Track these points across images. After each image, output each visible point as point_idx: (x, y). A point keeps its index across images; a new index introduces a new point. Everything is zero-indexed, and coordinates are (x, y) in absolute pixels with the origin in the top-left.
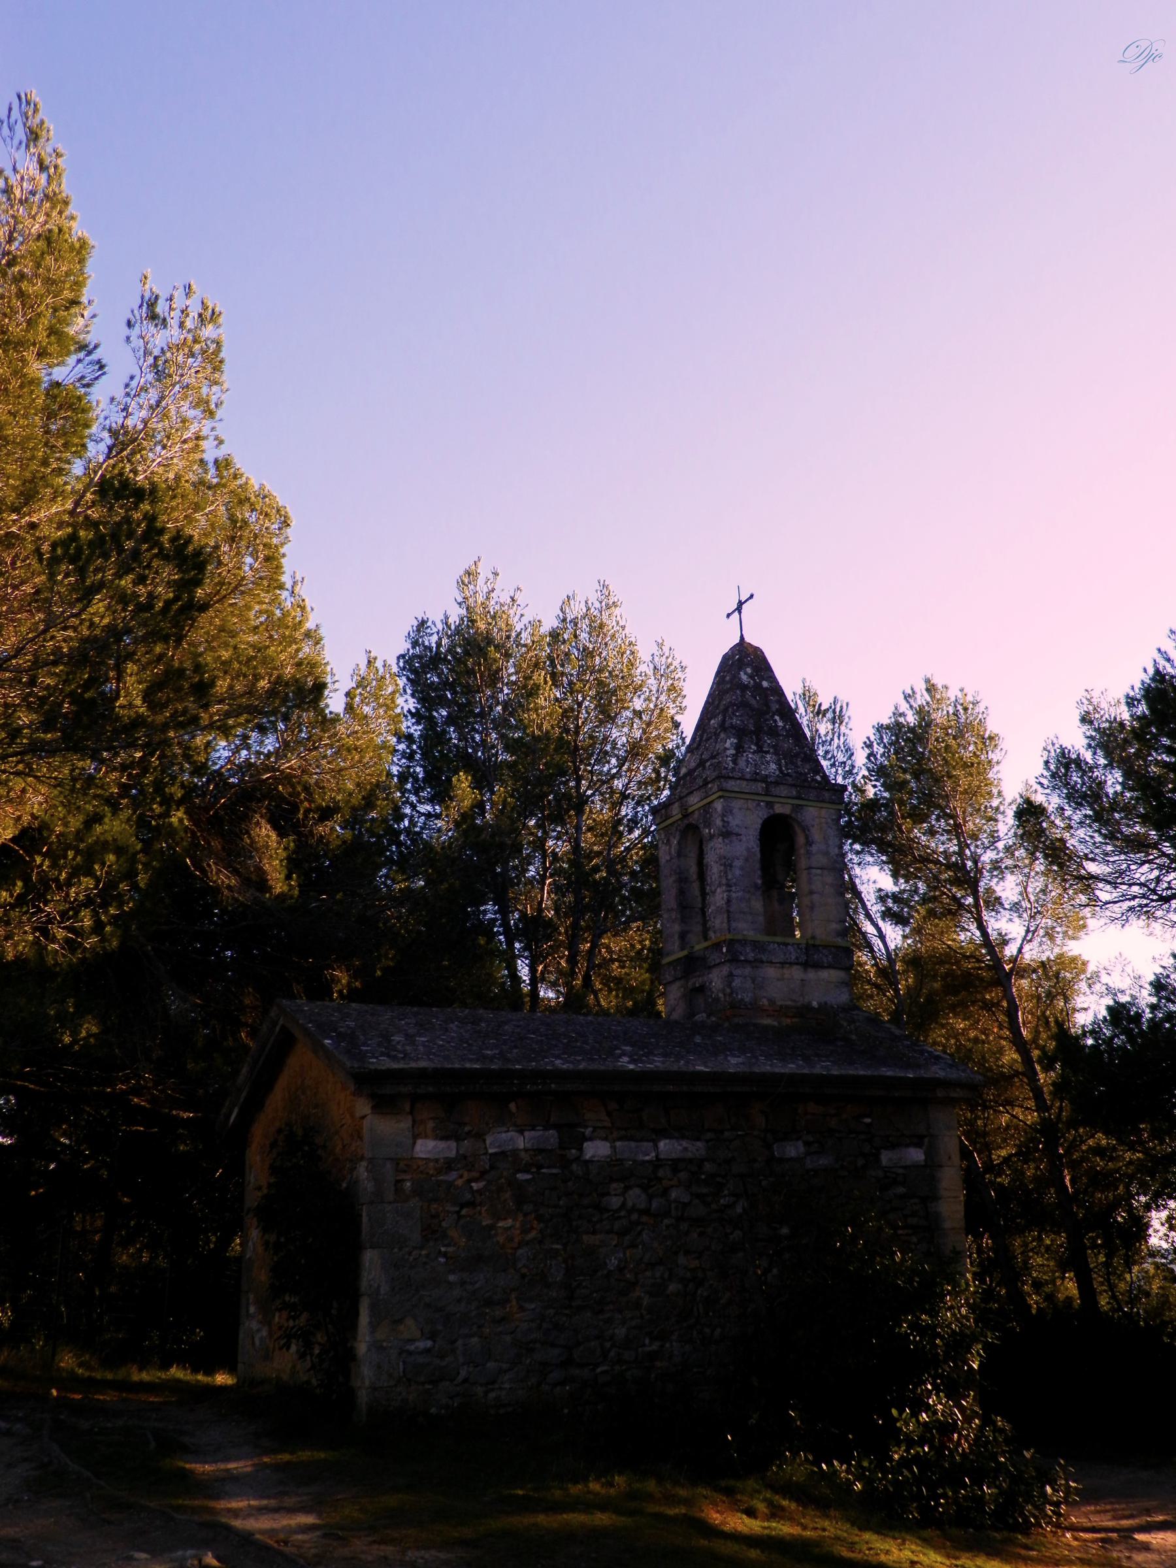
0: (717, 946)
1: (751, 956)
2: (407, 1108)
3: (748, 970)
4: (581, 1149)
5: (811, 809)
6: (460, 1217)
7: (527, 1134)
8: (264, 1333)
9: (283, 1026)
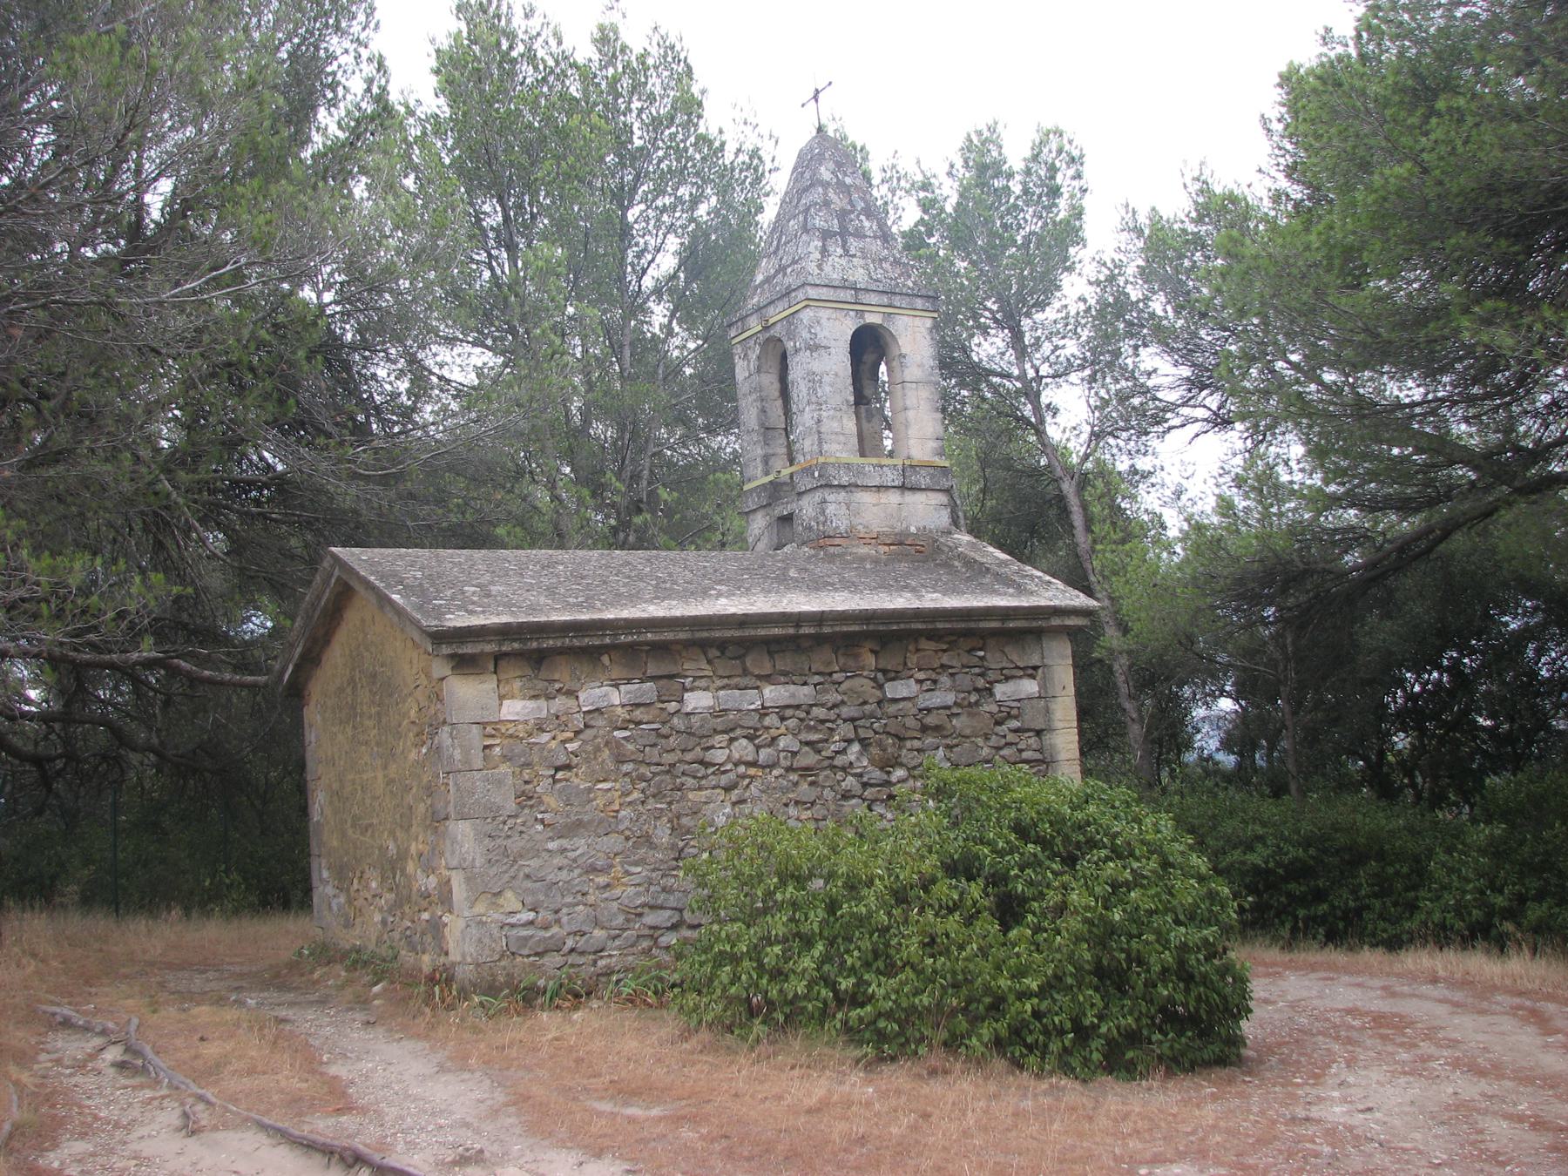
0: (808, 471)
1: (845, 480)
2: (491, 668)
3: (842, 495)
4: (681, 701)
5: (905, 318)
6: (555, 781)
7: (622, 688)
8: (342, 899)
9: (339, 579)
